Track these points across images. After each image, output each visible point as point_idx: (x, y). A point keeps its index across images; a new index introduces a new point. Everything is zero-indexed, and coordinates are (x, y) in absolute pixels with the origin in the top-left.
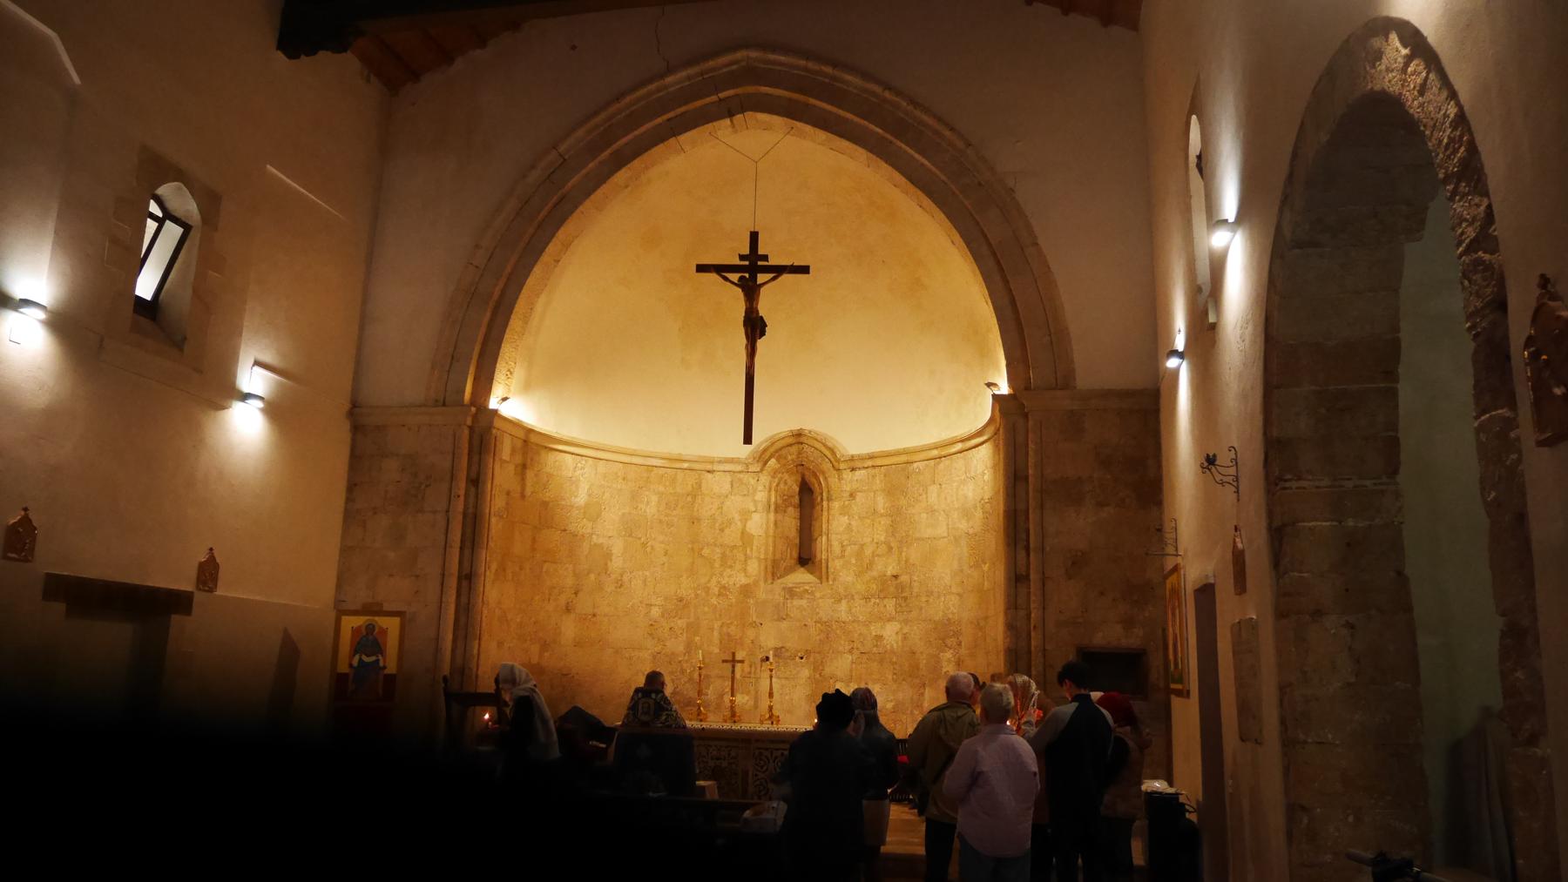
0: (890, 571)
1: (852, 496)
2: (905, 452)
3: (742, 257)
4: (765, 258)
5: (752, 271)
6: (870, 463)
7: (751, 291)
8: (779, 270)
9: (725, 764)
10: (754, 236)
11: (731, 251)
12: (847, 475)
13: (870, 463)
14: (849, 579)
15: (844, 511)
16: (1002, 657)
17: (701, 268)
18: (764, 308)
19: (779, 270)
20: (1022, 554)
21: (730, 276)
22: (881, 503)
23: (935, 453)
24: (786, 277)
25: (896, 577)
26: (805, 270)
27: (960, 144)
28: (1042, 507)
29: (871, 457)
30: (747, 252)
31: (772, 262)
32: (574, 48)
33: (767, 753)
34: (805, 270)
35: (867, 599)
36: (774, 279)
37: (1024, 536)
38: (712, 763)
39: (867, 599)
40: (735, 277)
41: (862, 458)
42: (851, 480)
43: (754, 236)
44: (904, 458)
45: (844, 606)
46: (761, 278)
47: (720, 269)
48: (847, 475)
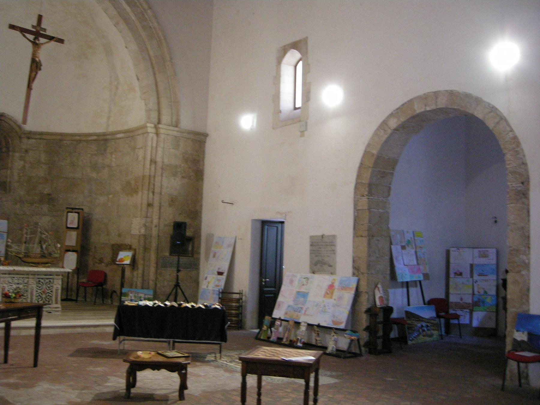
0: (46, 191)
1: (27, 151)
2: (61, 134)
3: (33, 27)
4: (45, 30)
5: (37, 34)
6: (39, 137)
7: (35, 45)
8: (51, 38)
9: (21, 286)
10: (40, 18)
11: (29, 24)
12: (25, 141)
13: (39, 137)
14: (22, 193)
15: (22, 158)
16: (169, 239)
17: (12, 27)
18: (42, 56)
19: (51, 38)
20: (151, 194)
21: (28, 36)
22: (43, 157)
23: (78, 138)
24: (53, 43)
25: (49, 194)
26: (61, 41)
27: (146, 7)
28: (162, 176)
29: (42, 134)
30: (35, 24)
31: (48, 33)
32: (254, 13)
33: (42, 281)
34: (61, 41)
35: (32, 204)
36: (47, 42)
37: (152, 186)
38: (14, 286)
39: (32, 204)
40: (31, 37)
41: (35, 133)
42: (26, 143)
43: (40, 18)
44: (59, 137)
45: (18, 206)
46: (42, 40)
47: (23, 31)
48: (25, 141)
